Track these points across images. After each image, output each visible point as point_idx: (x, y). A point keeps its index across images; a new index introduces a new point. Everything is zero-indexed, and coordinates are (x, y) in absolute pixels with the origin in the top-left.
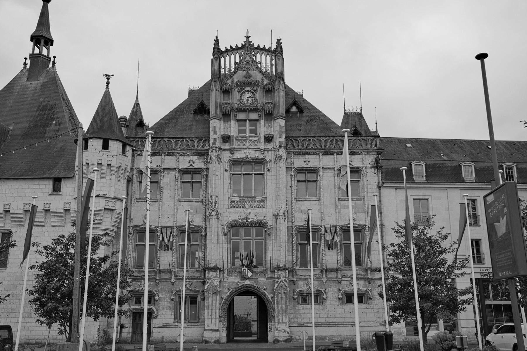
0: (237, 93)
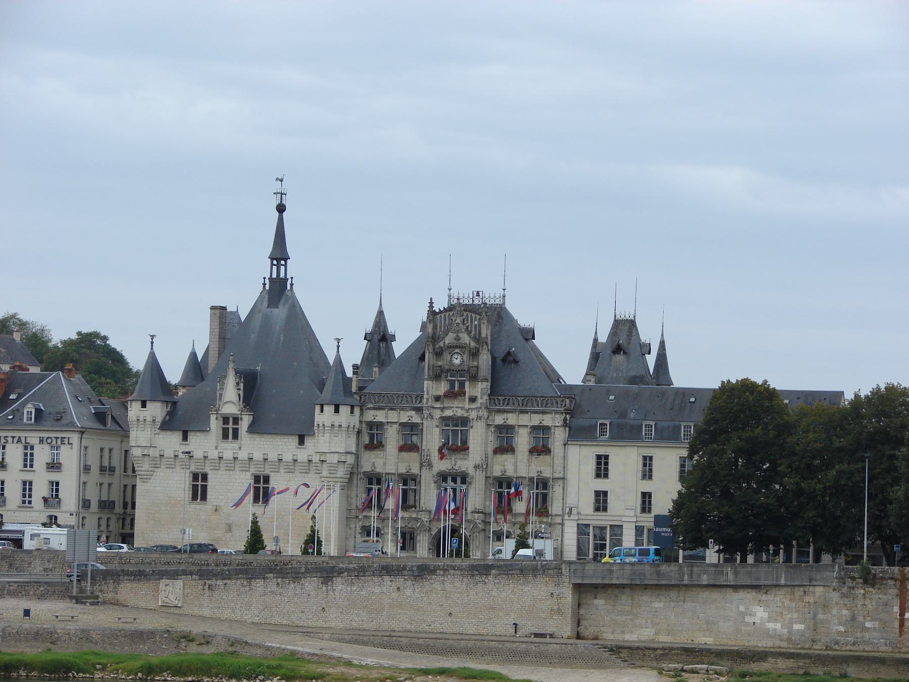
0: (448, 355)
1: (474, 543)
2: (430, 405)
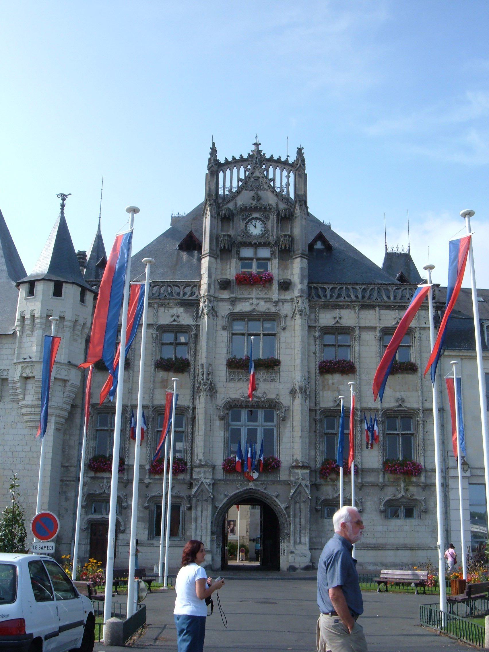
0: (241, 221)
1: (297, 520)
2: (212, 295)
